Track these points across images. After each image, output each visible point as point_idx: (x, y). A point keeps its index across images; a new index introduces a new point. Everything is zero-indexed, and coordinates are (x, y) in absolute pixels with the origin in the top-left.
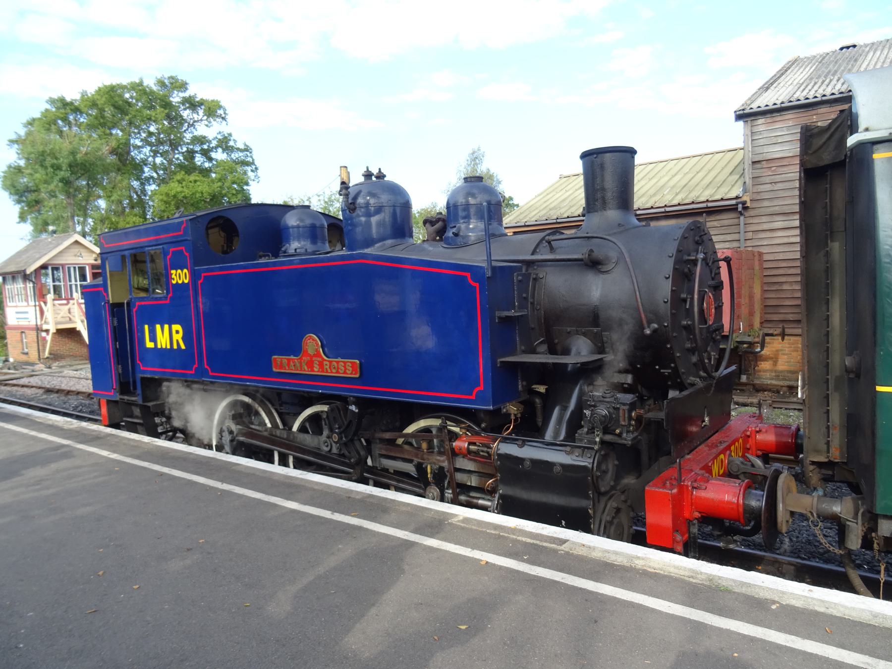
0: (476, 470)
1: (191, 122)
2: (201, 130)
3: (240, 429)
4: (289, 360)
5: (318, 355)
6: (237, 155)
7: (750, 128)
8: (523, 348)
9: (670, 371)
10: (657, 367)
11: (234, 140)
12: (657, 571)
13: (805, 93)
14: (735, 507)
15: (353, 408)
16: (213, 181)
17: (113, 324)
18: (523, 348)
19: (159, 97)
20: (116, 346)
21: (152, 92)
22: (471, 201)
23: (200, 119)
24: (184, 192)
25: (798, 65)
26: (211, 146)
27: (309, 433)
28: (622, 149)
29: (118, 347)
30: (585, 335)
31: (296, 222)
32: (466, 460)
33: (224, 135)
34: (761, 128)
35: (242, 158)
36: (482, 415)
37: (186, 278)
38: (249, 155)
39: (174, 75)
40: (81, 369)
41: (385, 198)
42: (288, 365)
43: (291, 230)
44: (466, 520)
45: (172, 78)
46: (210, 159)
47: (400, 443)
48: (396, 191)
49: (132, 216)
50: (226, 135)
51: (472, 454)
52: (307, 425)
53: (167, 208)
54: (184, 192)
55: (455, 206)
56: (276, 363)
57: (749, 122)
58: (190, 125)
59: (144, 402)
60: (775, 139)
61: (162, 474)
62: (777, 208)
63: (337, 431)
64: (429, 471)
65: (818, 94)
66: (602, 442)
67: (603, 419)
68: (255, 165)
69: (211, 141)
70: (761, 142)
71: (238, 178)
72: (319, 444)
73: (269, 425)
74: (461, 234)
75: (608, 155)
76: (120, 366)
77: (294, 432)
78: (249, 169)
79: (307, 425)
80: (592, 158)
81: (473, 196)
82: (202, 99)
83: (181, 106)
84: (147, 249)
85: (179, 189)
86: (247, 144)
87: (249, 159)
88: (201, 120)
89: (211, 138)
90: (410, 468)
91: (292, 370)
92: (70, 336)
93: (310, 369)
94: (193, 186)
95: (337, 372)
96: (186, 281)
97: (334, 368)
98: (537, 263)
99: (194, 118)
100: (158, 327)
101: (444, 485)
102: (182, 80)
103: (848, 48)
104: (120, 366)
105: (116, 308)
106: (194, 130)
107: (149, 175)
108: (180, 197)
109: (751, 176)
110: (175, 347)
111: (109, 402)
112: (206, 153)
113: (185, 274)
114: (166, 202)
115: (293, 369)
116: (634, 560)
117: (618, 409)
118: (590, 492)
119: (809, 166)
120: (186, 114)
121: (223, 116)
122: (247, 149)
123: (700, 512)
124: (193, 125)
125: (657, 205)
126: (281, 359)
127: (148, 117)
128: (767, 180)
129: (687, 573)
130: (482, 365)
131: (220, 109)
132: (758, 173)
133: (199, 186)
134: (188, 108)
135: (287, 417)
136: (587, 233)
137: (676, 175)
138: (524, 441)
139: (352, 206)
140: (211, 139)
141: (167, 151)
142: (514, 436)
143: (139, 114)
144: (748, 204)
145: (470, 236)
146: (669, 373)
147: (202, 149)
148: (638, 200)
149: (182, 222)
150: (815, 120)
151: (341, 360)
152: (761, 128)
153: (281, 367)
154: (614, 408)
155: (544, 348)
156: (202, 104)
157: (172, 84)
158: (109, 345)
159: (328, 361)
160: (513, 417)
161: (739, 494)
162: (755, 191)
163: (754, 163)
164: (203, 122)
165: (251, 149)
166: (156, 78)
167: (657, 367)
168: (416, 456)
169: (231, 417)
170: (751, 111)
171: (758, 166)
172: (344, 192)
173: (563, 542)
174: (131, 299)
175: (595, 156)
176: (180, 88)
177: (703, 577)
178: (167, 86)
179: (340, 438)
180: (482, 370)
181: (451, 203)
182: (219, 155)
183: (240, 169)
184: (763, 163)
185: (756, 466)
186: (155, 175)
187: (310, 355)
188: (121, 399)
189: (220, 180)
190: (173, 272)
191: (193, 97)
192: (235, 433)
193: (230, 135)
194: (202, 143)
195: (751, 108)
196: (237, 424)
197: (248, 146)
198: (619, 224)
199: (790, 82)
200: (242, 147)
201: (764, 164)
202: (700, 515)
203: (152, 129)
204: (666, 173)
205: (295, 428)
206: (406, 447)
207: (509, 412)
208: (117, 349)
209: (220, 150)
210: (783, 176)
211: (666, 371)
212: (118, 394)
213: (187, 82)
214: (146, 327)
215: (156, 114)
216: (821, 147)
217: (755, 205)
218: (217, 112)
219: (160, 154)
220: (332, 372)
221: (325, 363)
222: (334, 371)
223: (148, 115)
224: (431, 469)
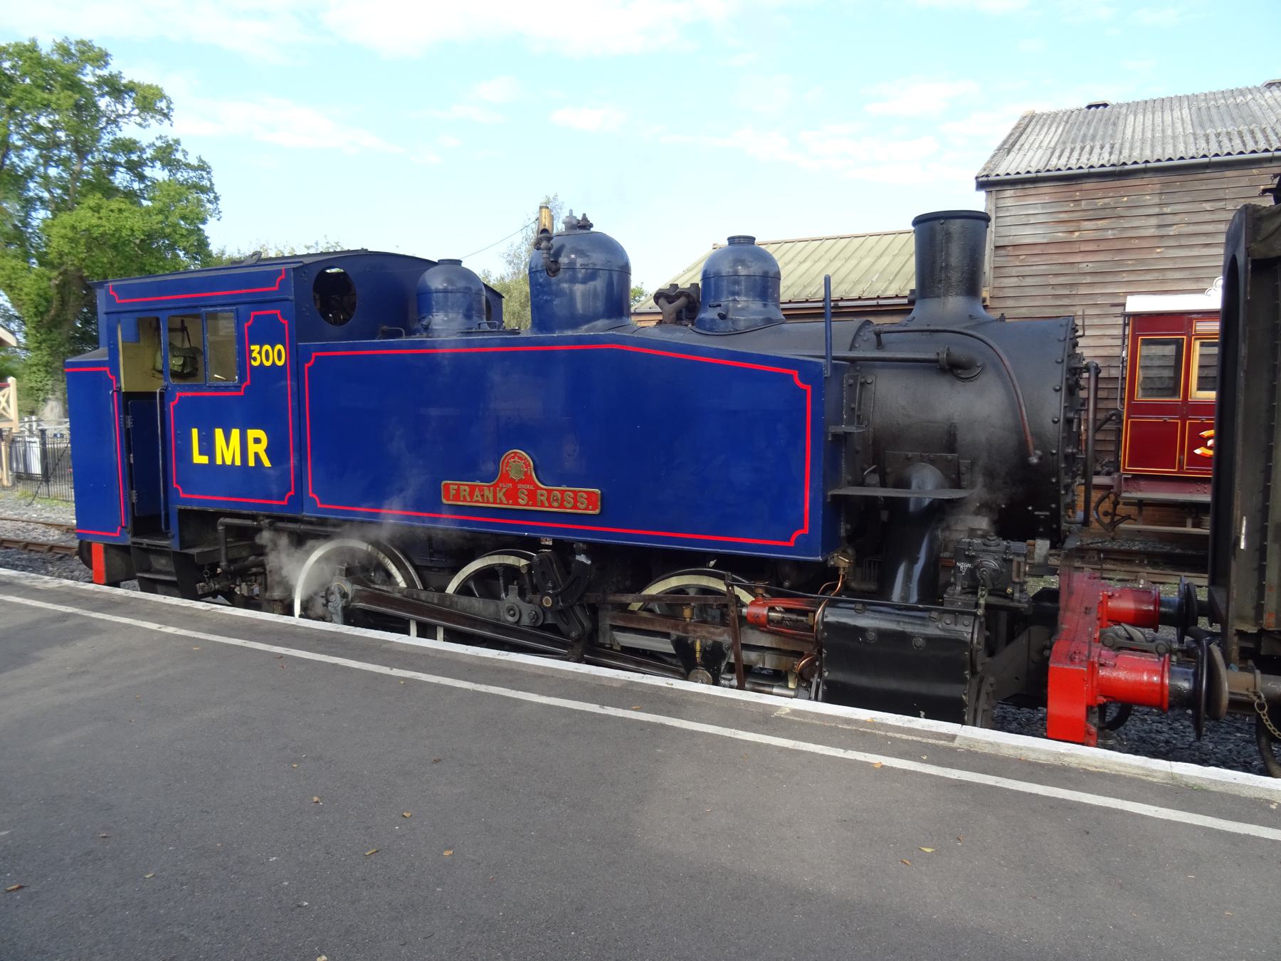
0: (774, 646)
1: (113, 116)
2: (129, 130)
3: (358, 591)
4: (472, 488)
5: (528, 480)
6: (185, 175)
7: (994, 200)
8: (850, 478)
9: (1048, 513)
10: (1030, 508)
11: (183, 151)
12: (1101, 770)
13: (1063, 160)
14: (1158, 688)
15: (582, 558)
16: (148, 211)
17: (125, 424)
18: (850, 478)
19: (63, 72)
20: (129, 460)
21: (50, 65)
22: (742, 270)
23: (127, 112)
24: (102, 226)
25: (1037, 122)
26: (145, 156)
27: (474, 595)
28: (973, 214)
29: (132, 461)
30: (932, 462)
31: (442, 285)
32: (757, 633)
33: (168, 141)
34: (1009, 202)
35: (194, 179)
36: (787, 569)
37: (280, 358)
38: (205, 176)
39: (86, 39)
41: (597, 258)
42: (471, 494)
43: (434, 295)
44: (795, 712)
45: (83, 43)
46: (142, 178)
47: (636, 609)
48: (608, 246)
49: (9, 258)
50: (171, 142)
51: (772, 624)
52: (473, 586)
53: (72, 248)
54: (102, 226)
55: (718, 276)
56: (447, 491)
57: (994, 193)
58: (111, 122)
59: (181, 549)
60: (1026, 219)
61: (281, 656)
62: (1023, 310)
63: (551, 592)
64: (698, 647)
65: (1082, 163)
66: (988, 607)
67: (993, 573)
68: (214, 192)
69: (144, 149)
70: (1008, 221)
71: (191, 211)
72: (498, 612)
73: (403, 584)
74: (730, 316)
75: (959, 222)
76: (134, 492)
77: (448, 595)
78: (204, 197)
79: (473, 586)
80: (927, 224)
81: (742, 262)
82: (131, 82)
83: (95, 89)
84: (203, 310)
85: (95, 221)
86: (203, 159)
87: (206, 183)
88: (130, 115)
89: (144, 144)
90: (665, 646)
91: (478, 501)
93: (511, 502)
94: (117, 218)
95: (562, 506)
96: (280, 363)
97: (556, 500)
98: (859, 362)
99: (117, 110)
100: (219, 433)
101: (719, 669)
102: (100, 49)
103: (1097, 106)
104: (134, 492)
105: (138, 404)
106: (116, 129)
107: (36, 194)
108: (96, 233)
109: (992, 266)
110: (252, 463)
111: (108, 547)
112: (135, 168)
113: (279, 351)
114: (71, 240)
115: (481, 500)
116: (1061, 757)
117: (1011, 561)
118: (966, 672)
119: (1257, 257)
120: (103, 103)
121: (166, 111)
122: (203, 167)
123: (1105, 697)
124: (115, 122)
125: (866, 295)
126: (459, 485)
127: (45, 102)
128: (1014, 271)
129: (1140, 772)
130: (808, 500)
131: (161, 101)
132: (1001, 261)
133: (126, 218)
134: (108, 93)
135: (425, 572)
136: (928, 325)
137: (881, 256)
138: (864, 604)
139: (554, 267)
140: (144, 146)
141: (69, 159)
142: (844, 597)
143: (29, 95)
144: (988, 303)
145: (739, 320)
146: (1045, 516)
147: (129, 161)
148: (836, 287)
149: (279, 272)
150: (1078, 198)
151: (567, 488)
152: (1009, 202)
153: (457, 497)
154: (1005, 560)
155: (875, 479)
156: (132, 90)
157: (83, 53)
158: (115, 453)
159: (545, 490)
160: (841, 572)
161: (1163, 670)
162: (996, 285)
163: (997, 247)
164: (132, 119)
165: (210, 168)
166: (54, 41)
167: (1030, 508)
168: (675, 627)
169: (344, 573)
170: (998, 178)
171: (1002, 252)
172: (544, 244)
173: (953, 738)
174: (167, 387)
175: (942, 221)
176: (98, 61)
177: (1161, 775)
178: (74, 55)
179: (555, 603)
180: (808, 505)
181: (712, 271)
182: (157, 173)
183: (193, 196)
184: (1009, 248)
185: (1135, 638)
186: (46, 195)
187: (512, 481)
188: (134, 543)
189: (161, 211)
190: (256, 348)
191: (116, 76)
192: (350, 597)
193: (177, 142)
194: (131, 152)
195: (998, 175)
196: (355, 582)
197: (202, 162)
198: (970, 316)
199: (1036, 145)
200: (195, 162)
201: (1010, 251)
202: (1105, 700)
203: (43, 121)
204: (868, 253)
205: (451, 589)
206: (645, 614)
207: (837, 565)
208: (131, 464)
209: (158, 164)
210: (1034, 268)
211: (1042, 514)
212: (129, 536)
213: (109, 52)
214: (195, 432)
215: (58, 99)
216: (1272, 234)
217: (996, 304)
218: (155, 104)
219: (55, 162)
220: (551, 506)
221: (539, 492)
222: (555, 504)
223: (44, 99)
224: (701, 646)
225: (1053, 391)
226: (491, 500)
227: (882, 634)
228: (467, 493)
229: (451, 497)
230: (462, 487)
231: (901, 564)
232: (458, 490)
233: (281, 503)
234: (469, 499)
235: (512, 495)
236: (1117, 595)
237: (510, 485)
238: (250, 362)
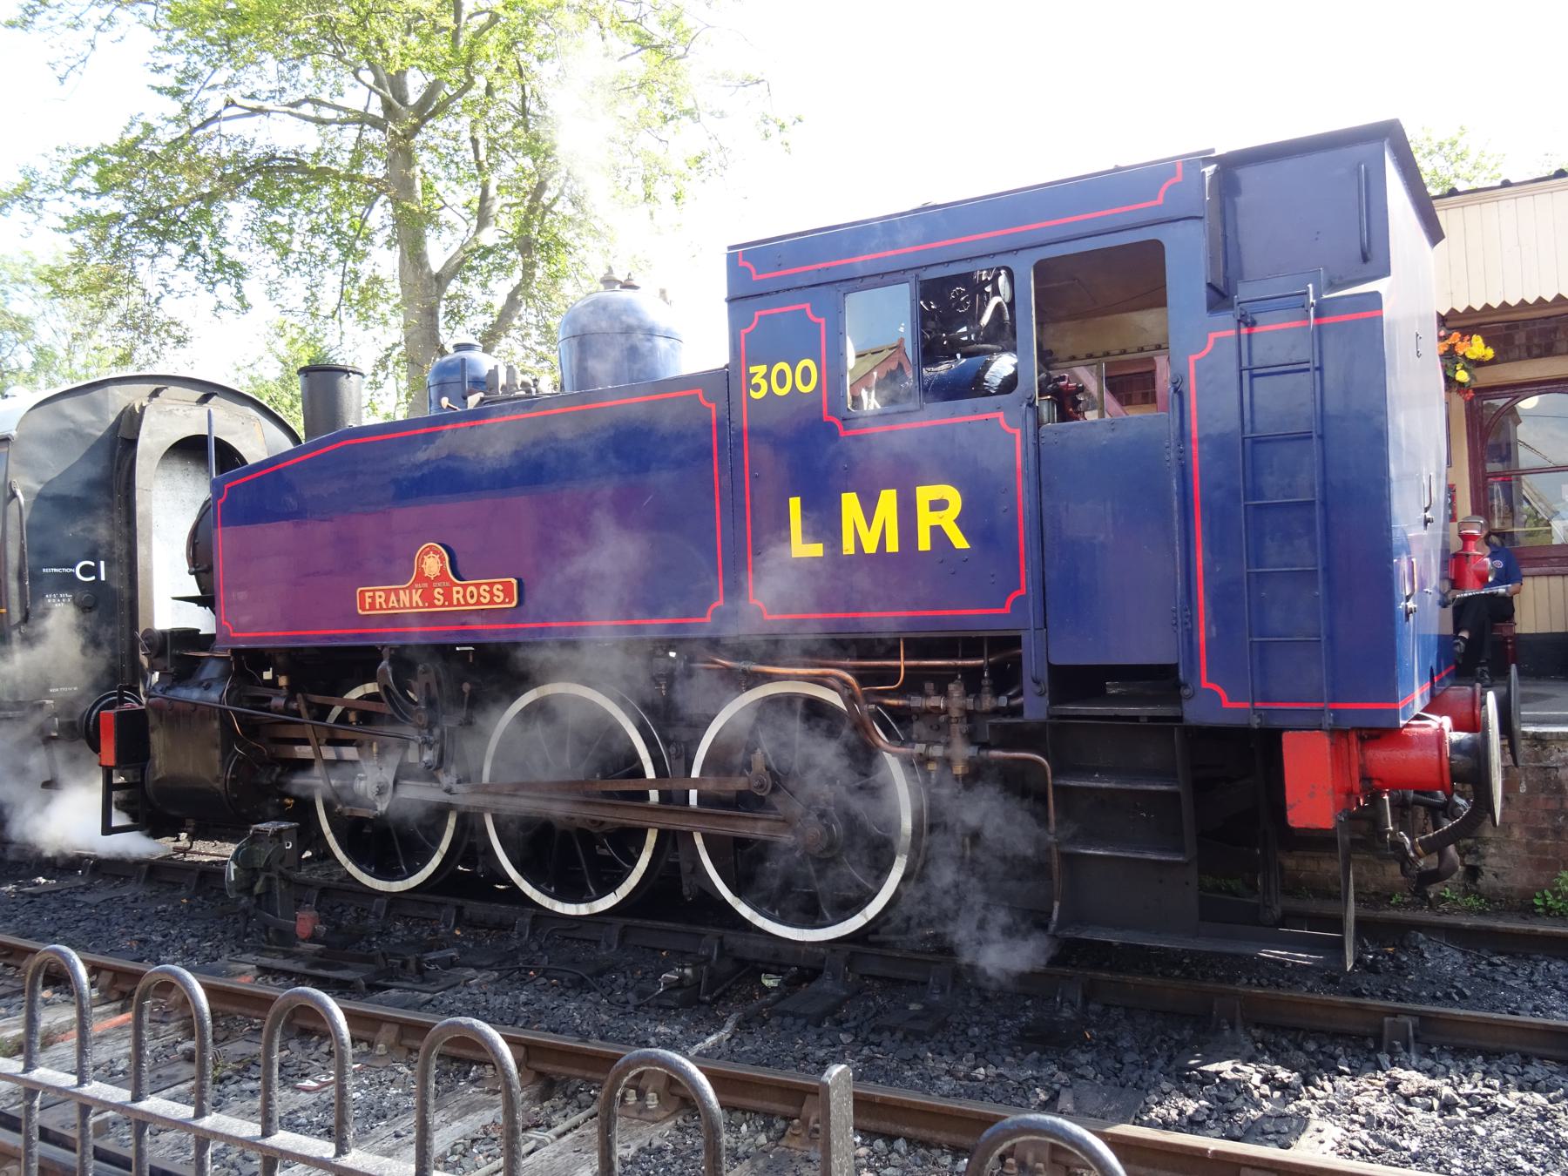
40: (922, 952)
42: (387, 601)
91: (393, 608)
92: (612, 432)
110: (924, 543)
113: (806, 371)
126: (374, 591)
153: (372, 606)
190: (761, 369)
220: (467, 604)
221: (455, 589)
227: (1152, 719)
228: (382, 600)
230: (377, 594)
232: (373, 598)
233: (1002, 611)
235: (427, 597)
237: (426, 585)
238: (748, 393)
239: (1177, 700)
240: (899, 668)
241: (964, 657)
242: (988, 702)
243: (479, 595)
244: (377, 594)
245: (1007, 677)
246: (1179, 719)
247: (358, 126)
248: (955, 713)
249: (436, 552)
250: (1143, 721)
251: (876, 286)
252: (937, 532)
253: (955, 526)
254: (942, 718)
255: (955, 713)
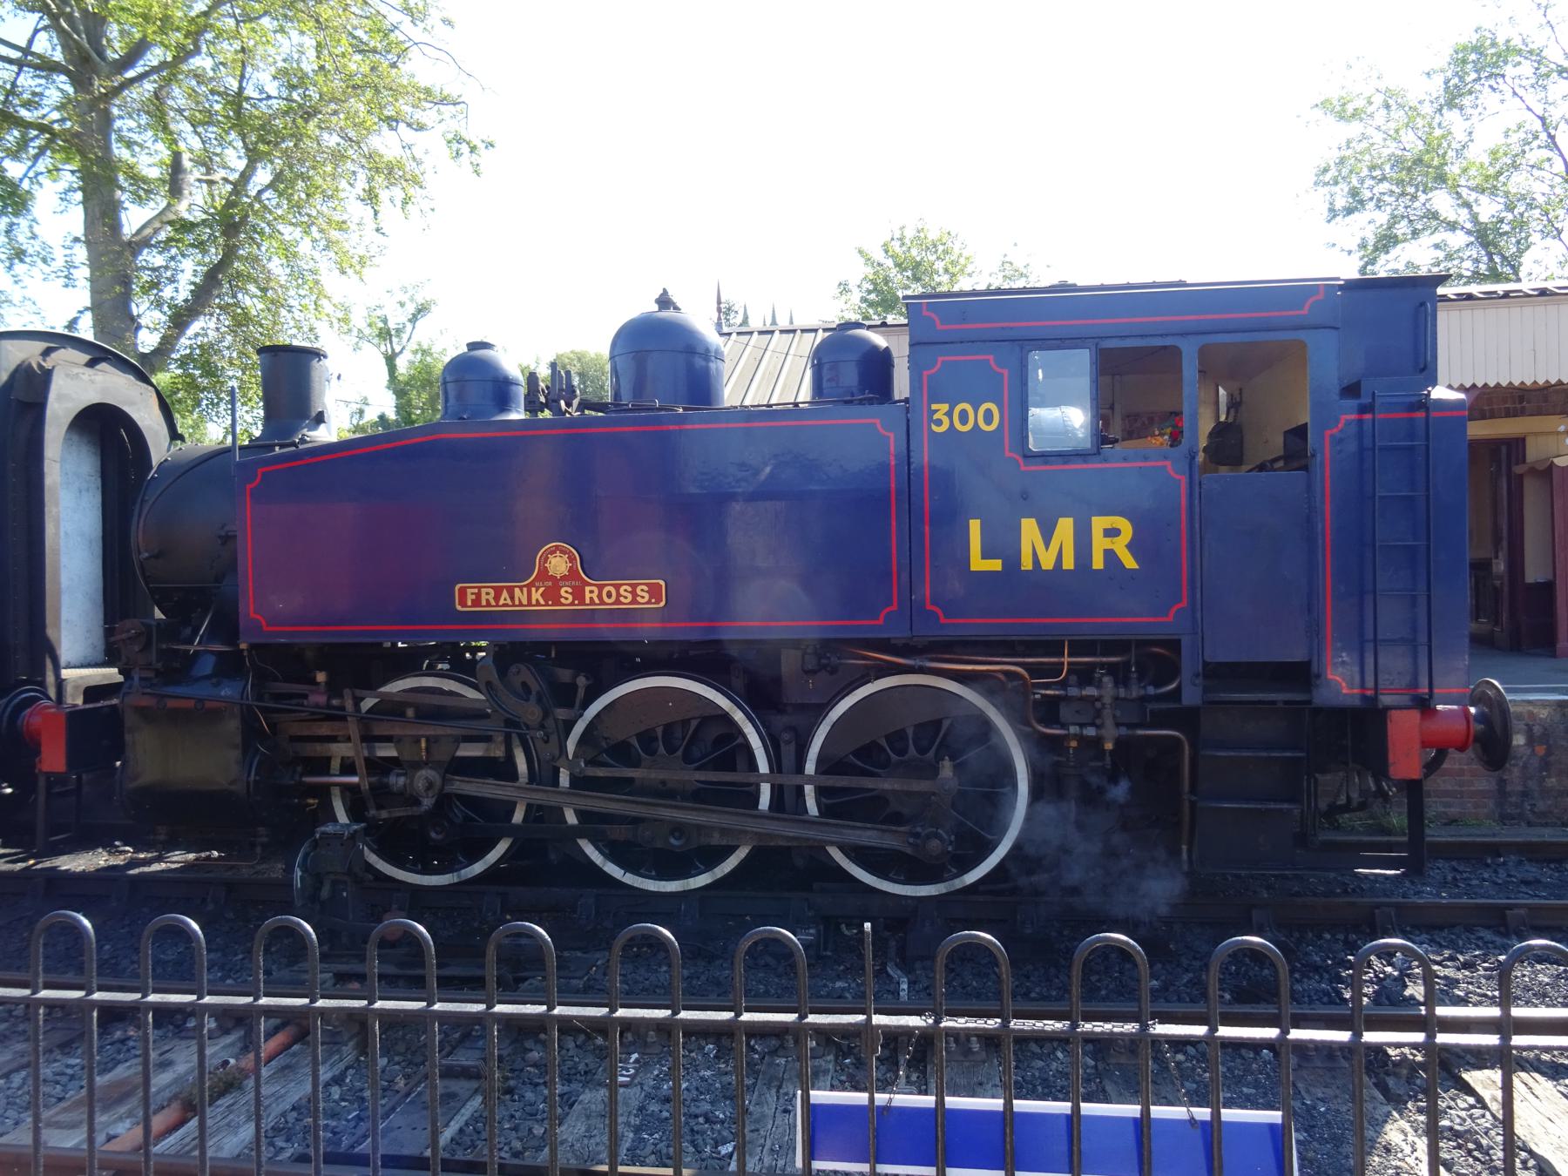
42: (497, 598)
91: (504, 605)
110: (1098, 563)
126: (479, 588)
153: (477, 602)
225: (1505, 130)
226: (525, 602)
227: (1286, 703)
229: (469, 603)
231: (45, 658)
232: (478, 595)
234: (493, 603)
235: (552, 595)
236: (829, 669)
239: (1309, 691)
240: (1063, 663)
241: (1103, 655)
242: (1135, 692)
243: (619, 595)
244: (484, 591)
245: (1169, 669)
246: (1309, 702)
247: (15, 68)
248: (1107, 700)
249: (563, 552)
250: (1280, 705)
251: (1059, 348)
252: (1110, 555)
253: (1126, 551)
254: (1098, 705)
255: (1107, 700)
